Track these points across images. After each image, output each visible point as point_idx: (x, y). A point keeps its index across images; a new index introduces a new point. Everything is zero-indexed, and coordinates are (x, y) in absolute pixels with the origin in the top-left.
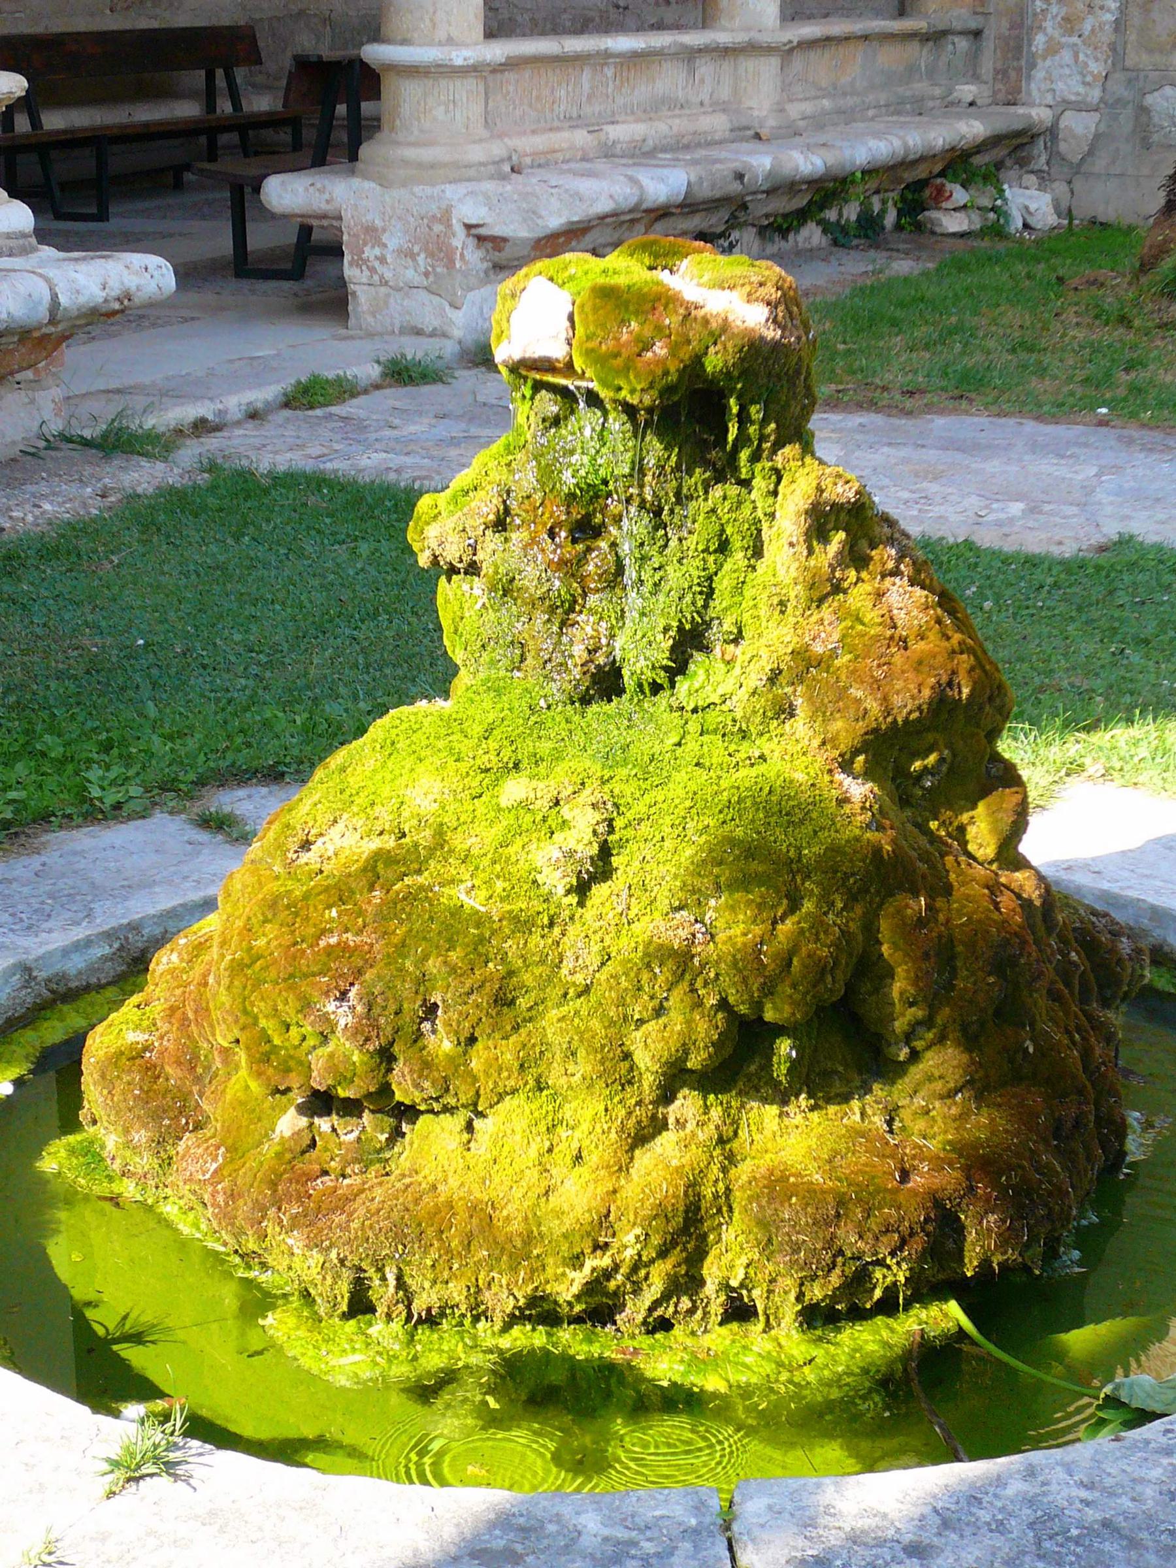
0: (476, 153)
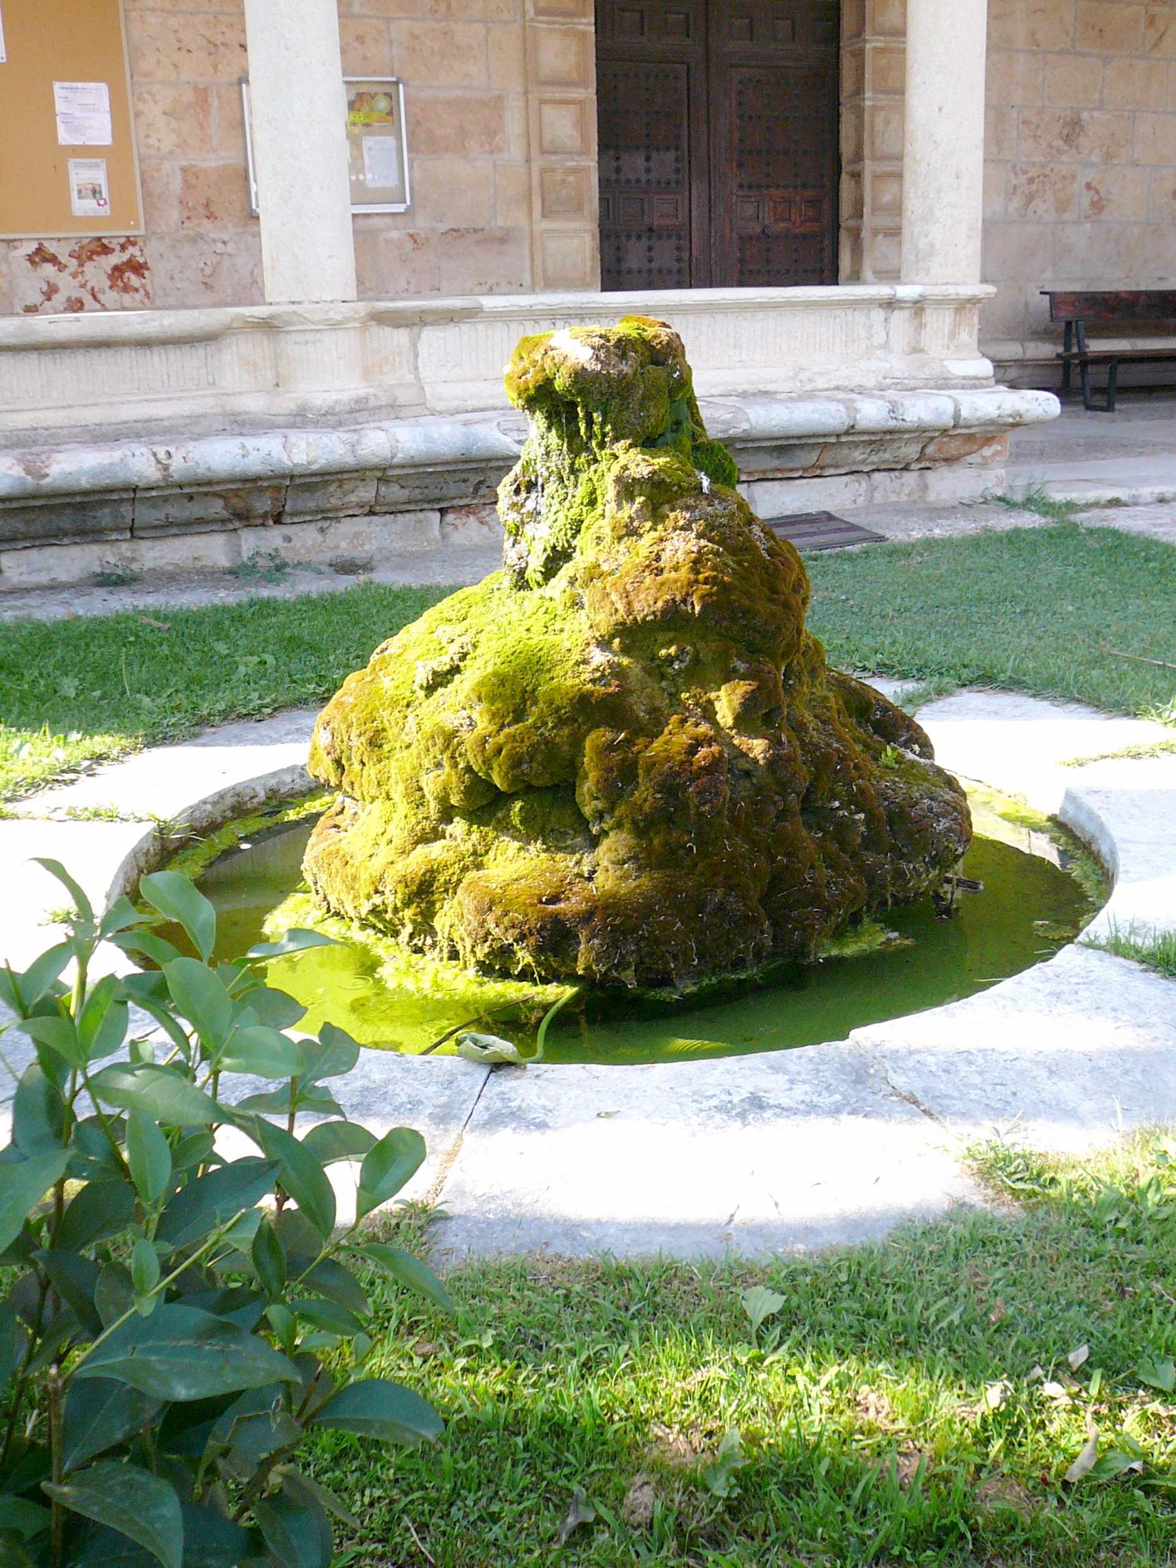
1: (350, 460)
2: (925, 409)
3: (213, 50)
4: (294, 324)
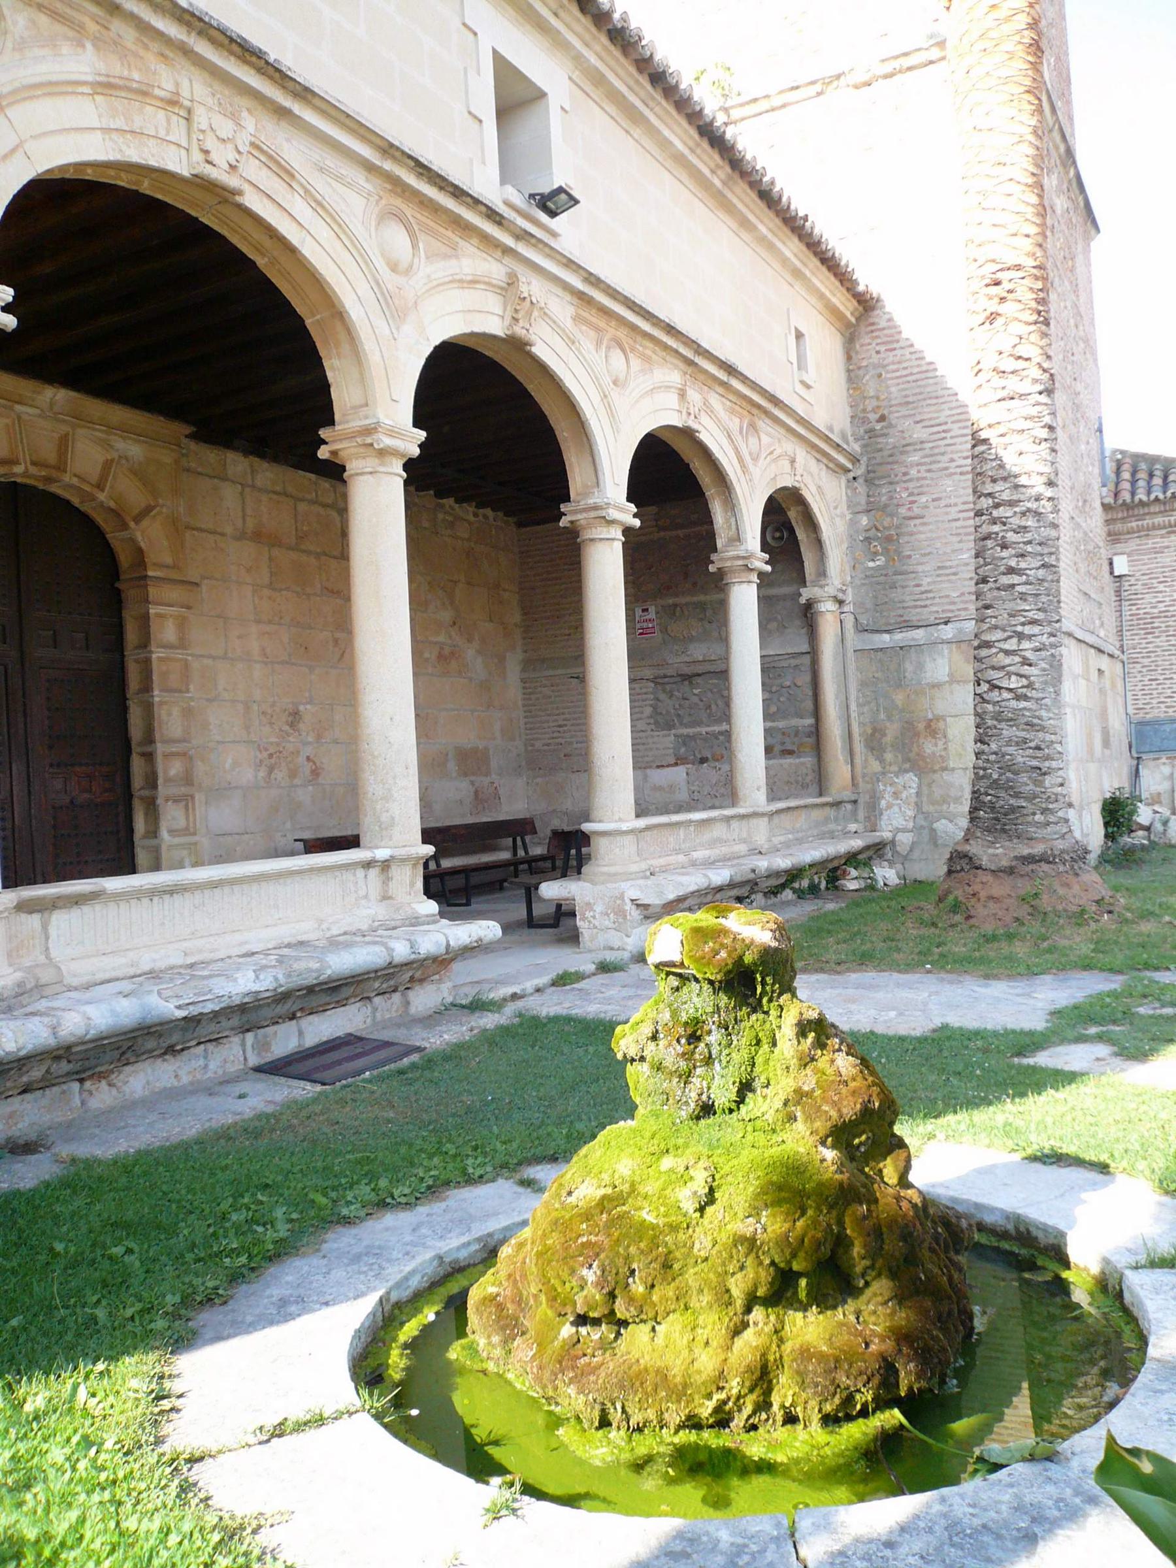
0: (634, 868)
1: (52, 1042)
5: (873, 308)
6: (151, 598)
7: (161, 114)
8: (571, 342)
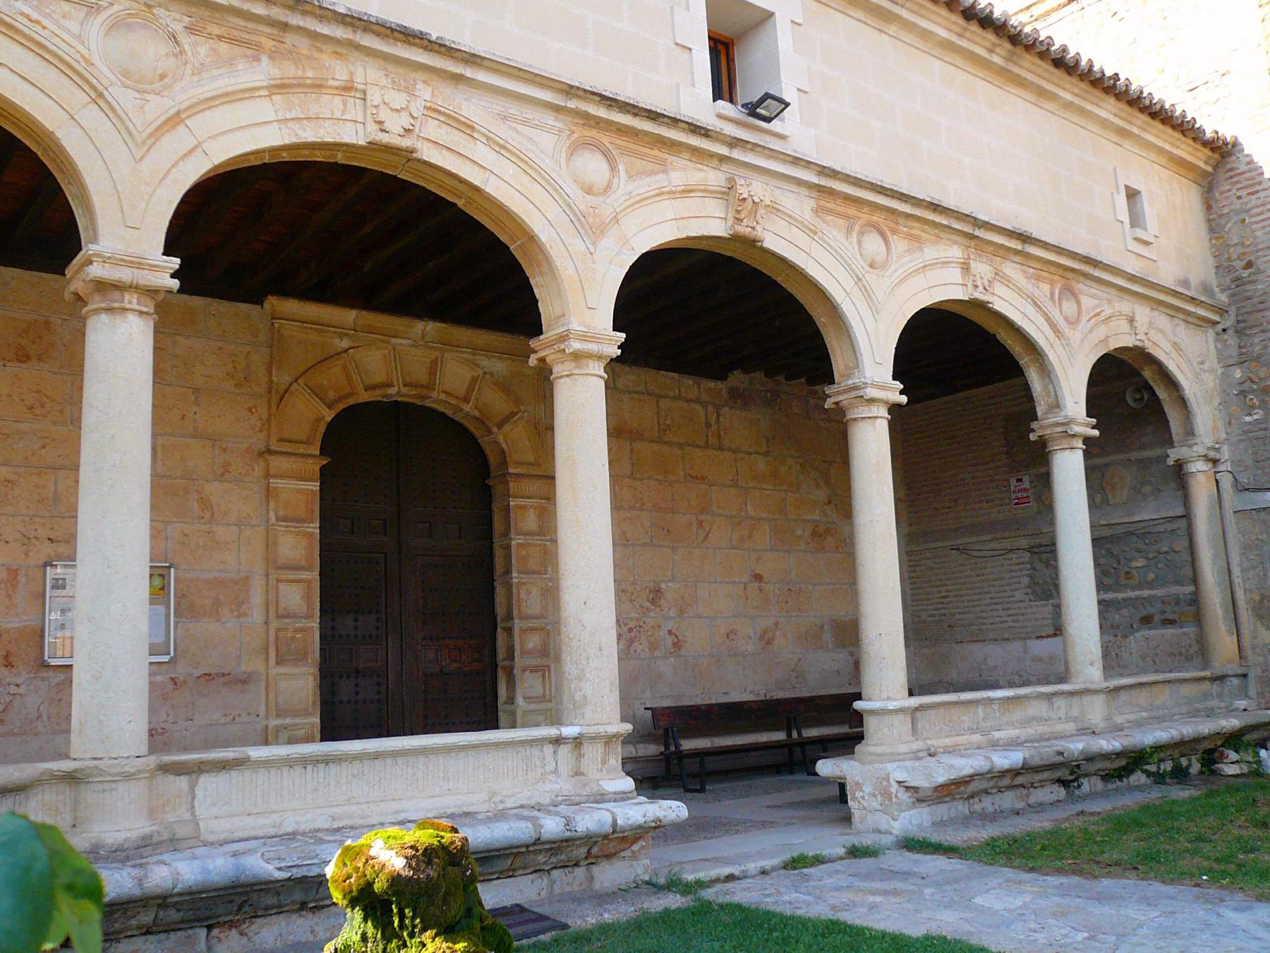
0: (904, 748)
1: (137, 892)
2: (591, 821)
3: (26, 541)
4: (95, 776)
5: (1229, 154)
6: (511, 492)
7: (338, 100)
8: (813, 233)
